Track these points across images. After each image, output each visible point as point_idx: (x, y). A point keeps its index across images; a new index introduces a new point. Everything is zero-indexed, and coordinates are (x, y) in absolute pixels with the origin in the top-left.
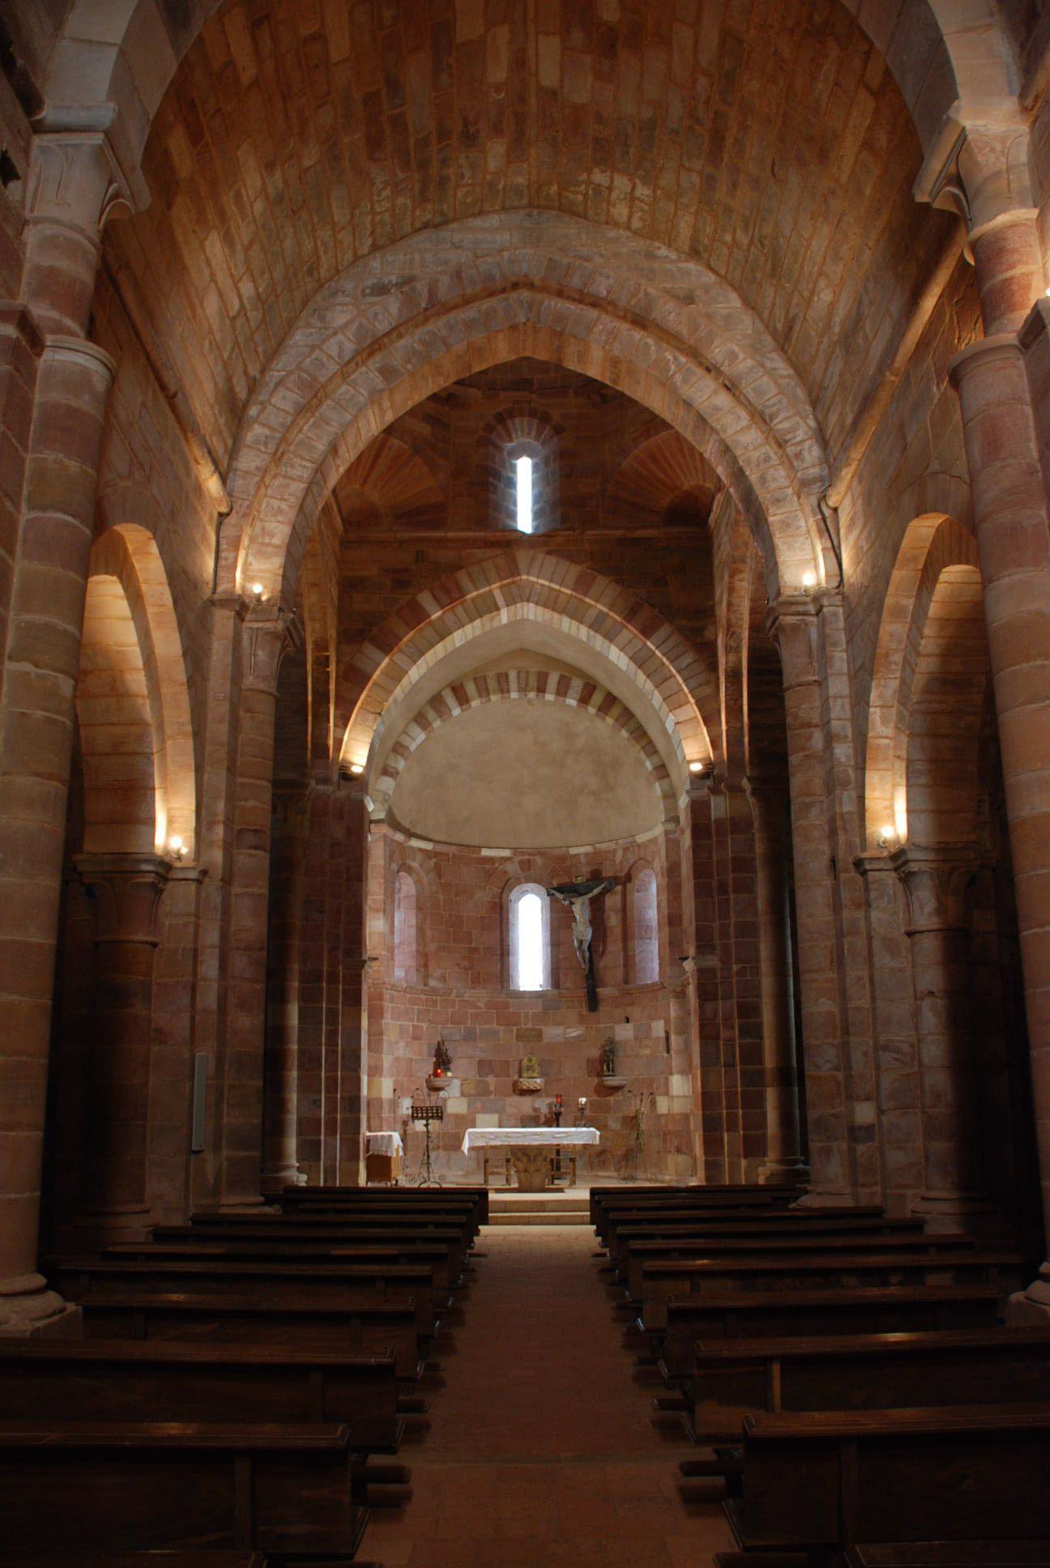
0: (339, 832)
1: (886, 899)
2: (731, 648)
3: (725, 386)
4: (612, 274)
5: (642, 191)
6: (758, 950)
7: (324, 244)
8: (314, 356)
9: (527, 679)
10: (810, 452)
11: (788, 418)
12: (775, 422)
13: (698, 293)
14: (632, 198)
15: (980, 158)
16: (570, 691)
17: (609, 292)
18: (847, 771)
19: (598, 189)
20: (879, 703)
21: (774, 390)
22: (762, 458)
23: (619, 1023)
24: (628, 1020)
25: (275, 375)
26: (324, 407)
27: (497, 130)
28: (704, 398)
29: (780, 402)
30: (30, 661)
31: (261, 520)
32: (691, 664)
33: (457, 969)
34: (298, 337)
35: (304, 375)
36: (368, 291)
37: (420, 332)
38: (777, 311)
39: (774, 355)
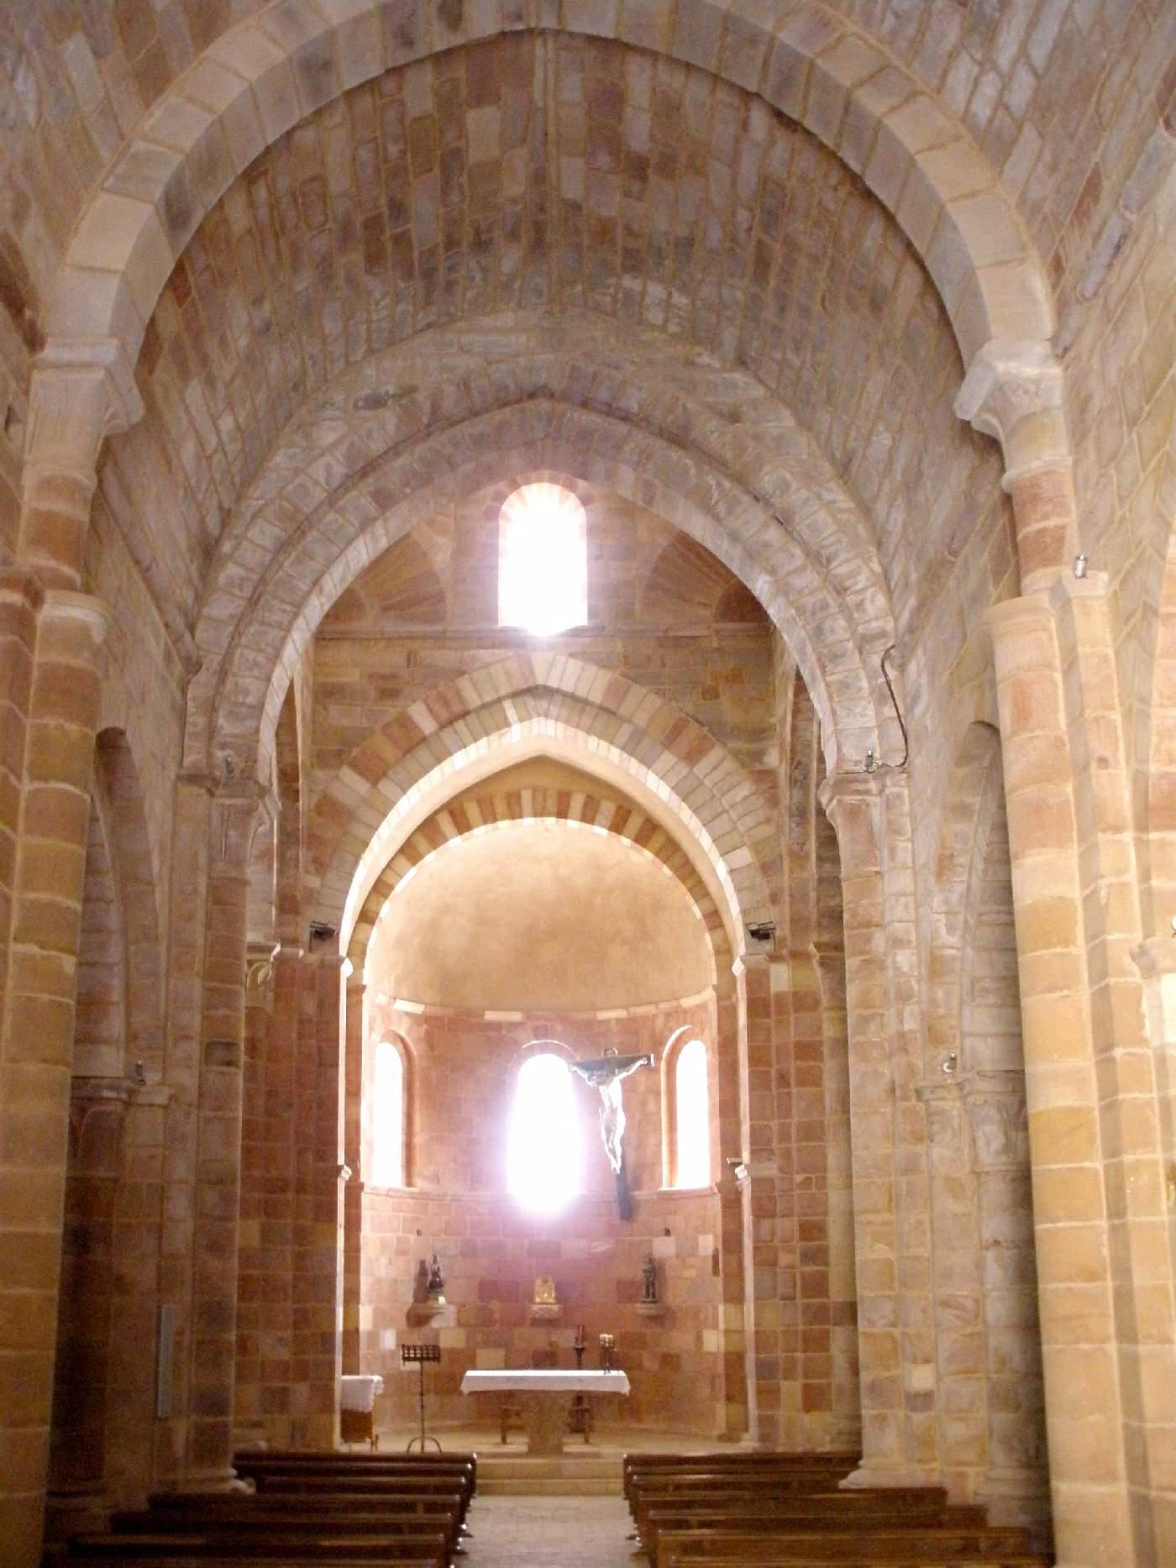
0: (310, 1007)
1: (950, 1132)
2: (796, 781)
3: (777, 519)
4: (645, 385)
5: (681, 300)
6: (824, 1156)
7: (312, 357)
8: (298, 481)
9: (545, 801)
10: (873, 601)
11: (847, 561)
12: (834, 564)
13: (745, 409)
14: (668, 305)
15: (1014, 399)
16: (599, 817)
17: (641, 407)
18: (909, 981)
19: (628, 295)
20: (944, 909)
21: (833, 528)
22: (818, 606)
23: (657, 1236)
24: (668, 1232)
25: (252, 504)
26: (309, 538)
27: (513, 235)
28: (752, 532)
29: (839, 542)
30: (36, 943)
31: (234, 675)
32: (747, 797)
33: (452, 1165)
34: (280, 458)
35: (285, 504)
36: (360, 404)
37: (420, 450)
38: (834, 437)
39: (832, 485)
